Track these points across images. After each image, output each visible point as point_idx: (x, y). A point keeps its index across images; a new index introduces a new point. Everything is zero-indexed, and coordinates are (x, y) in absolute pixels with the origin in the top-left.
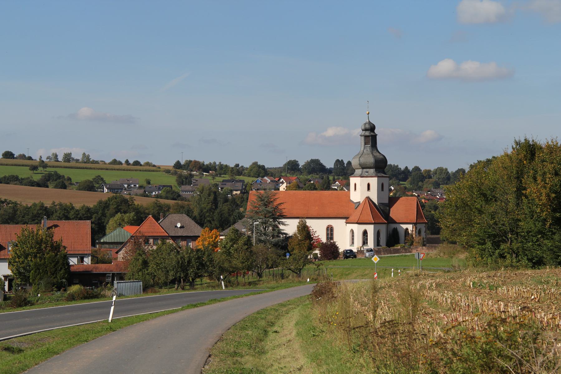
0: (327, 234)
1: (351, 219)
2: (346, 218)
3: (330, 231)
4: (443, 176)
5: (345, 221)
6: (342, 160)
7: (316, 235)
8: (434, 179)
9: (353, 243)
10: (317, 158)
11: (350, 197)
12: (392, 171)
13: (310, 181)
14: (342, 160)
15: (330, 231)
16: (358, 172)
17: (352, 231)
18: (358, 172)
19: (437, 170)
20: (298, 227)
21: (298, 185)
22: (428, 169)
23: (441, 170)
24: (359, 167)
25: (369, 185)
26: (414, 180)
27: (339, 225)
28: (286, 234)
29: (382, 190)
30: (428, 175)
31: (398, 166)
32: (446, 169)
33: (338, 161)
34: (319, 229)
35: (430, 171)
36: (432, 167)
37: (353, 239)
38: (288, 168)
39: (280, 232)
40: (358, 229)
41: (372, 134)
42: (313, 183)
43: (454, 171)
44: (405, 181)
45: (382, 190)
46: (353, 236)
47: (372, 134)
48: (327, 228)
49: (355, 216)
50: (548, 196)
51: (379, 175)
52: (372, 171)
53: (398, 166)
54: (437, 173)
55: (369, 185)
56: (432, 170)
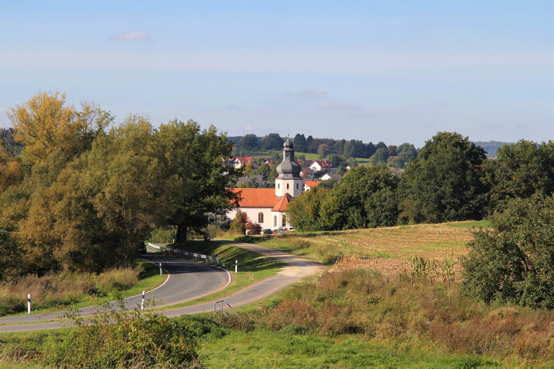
0: (259, 218)
1: (275, 208)
2: (272, 208)
3: (261, 217)
4: (409, 152)
5: (271, 209)
9: (276, 224)
11: (275, 193)
12: (356, 147)
13: (265, 161)
14: (303, 135)
15: (261, 217)
16: (281, 175)
17: (275, 217)
18: (281, 175)
19: (402, 146)
20: (237, 215)
21: (252, 166)
22: (393, 145)
24: (281, 172)
25: (288, 185)
26: (377, 157)
27: (267, 212)
28: (229, 219)
29: (297, 188)
30: (394, 151)
31: (361, 141)
32: (413, 146)
33: (298, 135)
34: (252, 215)
35: (395, 147)
39: (226, 218)
44: (368, 158)
45: (297, 188)
48: (259, 214)
49: (277, 207)
50: (312, 210)
52: (290, 176)
53: (361, 141)
55: (288, 185)
56: (398, 146)
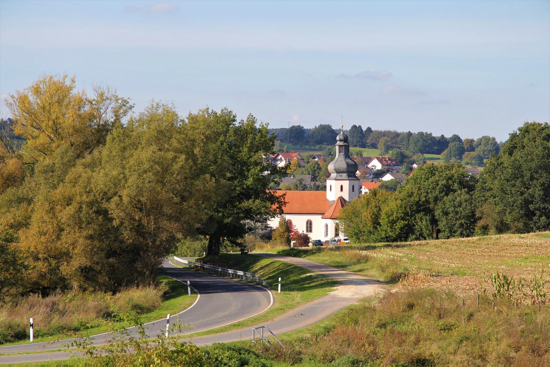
0: (307, 227)
3: (309, 225)
4: (489, 147)
5: (321, 216)
6: (360, 126)
7: (296, 228)
8: (478, 151)
9: (327, 235)
10: (327, 124)
14: (360, 126)
15: (309, 225)
18: (334, 175)
19: (481, 139)
20: (280, 223)
22: (470, 138)
23: (486, 139)
24: (334, 171)
25: (342, 187)
27: (317, 220)
28: (271, 227)
29: (353, 190)
30: (471, 146)
31: (431, 134)
32: (494, 139)
33: (355, 126)
34: (299, 223)
35: (472, 141)
36: (476, 137)
37: (327, 232)
38: (290, 136)
39: (266, 227)
40: (331, 224)
41: (346, 144)
42: (318, 161)
43: (504, 142)
44: (440, 154)
45: (353, 190)
46: (327, 229)
47: (346, 144)
48: (307, 222)
49: (329, 213)
50: (371, 217)
51: (350, 178)
52: (345, 175)
53: (431, 134)
54: (482, 143)
55: (342, 187)
56: (475, 140)
